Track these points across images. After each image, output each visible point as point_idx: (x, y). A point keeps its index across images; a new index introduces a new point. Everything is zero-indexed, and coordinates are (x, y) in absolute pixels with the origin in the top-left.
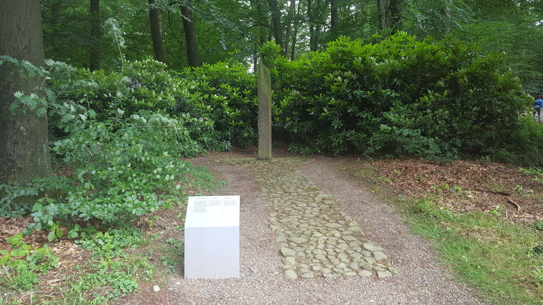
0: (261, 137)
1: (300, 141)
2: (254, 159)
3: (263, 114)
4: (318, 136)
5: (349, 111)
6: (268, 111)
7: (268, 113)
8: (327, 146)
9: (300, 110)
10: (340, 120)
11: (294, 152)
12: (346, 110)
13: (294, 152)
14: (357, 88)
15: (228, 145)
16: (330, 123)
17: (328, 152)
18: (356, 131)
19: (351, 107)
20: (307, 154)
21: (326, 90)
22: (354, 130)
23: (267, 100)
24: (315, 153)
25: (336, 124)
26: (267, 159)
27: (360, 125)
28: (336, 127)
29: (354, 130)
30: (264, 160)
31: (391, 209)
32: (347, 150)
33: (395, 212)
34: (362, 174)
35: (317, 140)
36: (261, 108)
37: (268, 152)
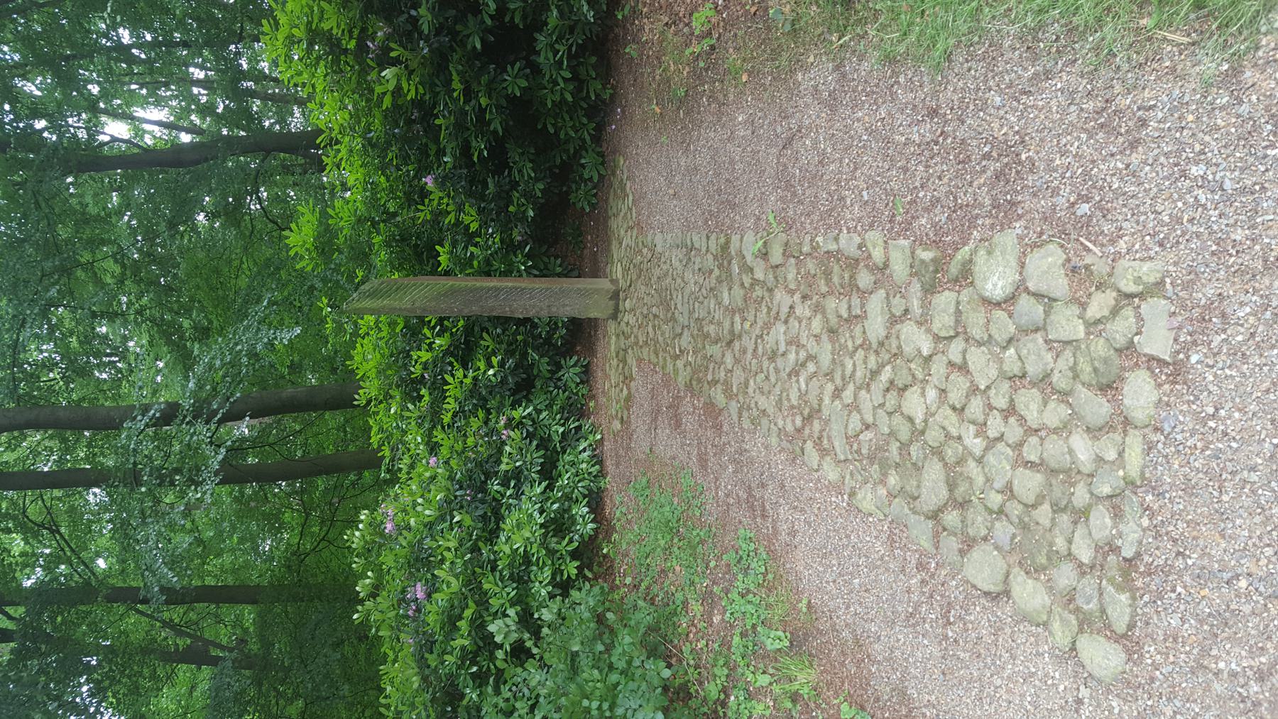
0: (554, 309)
1: (563, 175)
2: (612, 327)
3: (491, 303)
4: (552, 131)
5: (478, 46)
6: (482, 289)
7: (490, 289)
8: (582, 108)
9: (481, 174)
10: (505, 70)
11: (595, 195)
12: (475, 54)
13: (595, 195)
14: (414, 21)
15: (570, 374)
16: (512, 99)
17: (597, 113)
18: (540, 30)
19: (469, 36)
20: (603, 164)
21: (426, 110)
22: (537, 35)
23: (453, 292)
24: (597, 139)
25: (514, 82)
26: (615, 296)
27: (524, 17)
28: (524, 84)
29: (537, 35)
30: (617, 305)
31: (817, 74)
32: (594, 59)
33: (837, 68)
34: (676, 69)
35: (562, 136)
36: (475, 309)
37: (597, 291)
